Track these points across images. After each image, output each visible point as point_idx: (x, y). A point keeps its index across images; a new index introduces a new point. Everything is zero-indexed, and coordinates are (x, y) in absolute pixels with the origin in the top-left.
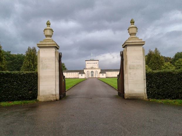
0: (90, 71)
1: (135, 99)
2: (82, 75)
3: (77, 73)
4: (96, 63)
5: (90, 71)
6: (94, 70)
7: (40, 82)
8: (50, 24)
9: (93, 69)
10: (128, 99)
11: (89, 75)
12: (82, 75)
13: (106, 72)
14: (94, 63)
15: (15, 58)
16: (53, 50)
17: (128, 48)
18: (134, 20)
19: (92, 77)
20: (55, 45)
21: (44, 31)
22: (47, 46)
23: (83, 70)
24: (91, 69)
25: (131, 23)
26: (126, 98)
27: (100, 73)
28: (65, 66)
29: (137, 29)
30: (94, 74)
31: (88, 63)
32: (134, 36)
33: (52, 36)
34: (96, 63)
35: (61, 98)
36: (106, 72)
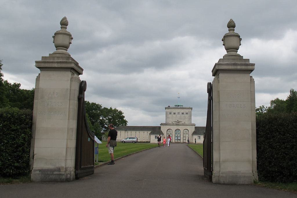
1: (232, 184)
3: (146, 132)
4: (187, 113)
5: (176, 127)
6: (182, 128)
7: (36, 140)
8: (234, 27)
9: (179, 125)
10: (218, 183)
14: (170, 113)
15: (28, 98)
16: (69, 74)
17: (221, 75)
18: (68, 20)
19: (176, 141)
20: (73, 65)
21: (54, 37)
22: (56, 65)
23: (160, 127)
24: (177, 125)
25: (229, 27)
26: (214, 180)
27: (194, 133)
28: (124, 117)
29: (240, 40)
30: (182, 136)
31: (170, 113)
32: (234, 53)
33: (70, 47)
34: (187, 113)
35: (77, 177)
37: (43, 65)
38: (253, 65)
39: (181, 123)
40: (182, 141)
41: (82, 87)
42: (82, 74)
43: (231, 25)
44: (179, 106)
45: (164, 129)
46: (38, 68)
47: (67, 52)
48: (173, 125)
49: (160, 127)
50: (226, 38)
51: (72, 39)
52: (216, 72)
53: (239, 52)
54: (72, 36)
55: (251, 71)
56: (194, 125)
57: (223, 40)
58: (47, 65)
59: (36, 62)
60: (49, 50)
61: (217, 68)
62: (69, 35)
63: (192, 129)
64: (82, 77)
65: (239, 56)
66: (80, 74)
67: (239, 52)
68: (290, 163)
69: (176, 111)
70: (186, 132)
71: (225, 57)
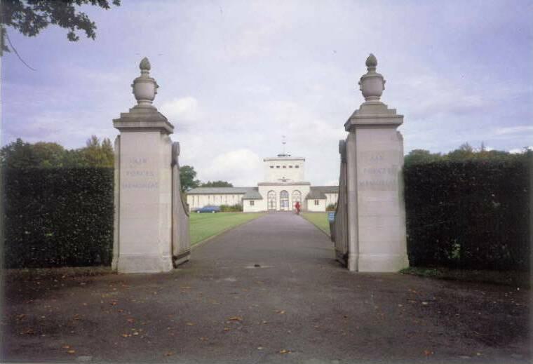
0: (278, 189)
2: (317, 203)
8: (148, 69)
11: (274, 204)
12: (317, 203)
13: (327, 195)
14: (272, 167)
17: (359, 132)
23: (256, 189)
29: (384, 82)
33: (156, 98)
34: (297, 167)
36: (327, 195)
37: (124, 125)
38: (402, 117)
39: (289, 182)
40: (278, 209)
41: (175, 151)
42: (172, 133)
43: (371, 63)
44: (284, 155)
45: (263, 191)
46: (118, 128)
47: (152, 105)
48: (275, 184)
49: (256, 189)
50: (138, 84)
51: (157, 87)
52: (351, 127)
53: (382, 100)
54: (385, 79)
55: (398, 125)
56: (308, 184)
57: (359, 84)
58: (131, 125)
59: (115, 121)
60: (127, 102)
61: (353, 122)
62: (380, 77)
63: (306, 190)
64: (174, 137)
65: (382, 104)
66: (169, 133)
67: (382, 100)
68: (425, 223)
69: (281, 164)
71: (363, 108)
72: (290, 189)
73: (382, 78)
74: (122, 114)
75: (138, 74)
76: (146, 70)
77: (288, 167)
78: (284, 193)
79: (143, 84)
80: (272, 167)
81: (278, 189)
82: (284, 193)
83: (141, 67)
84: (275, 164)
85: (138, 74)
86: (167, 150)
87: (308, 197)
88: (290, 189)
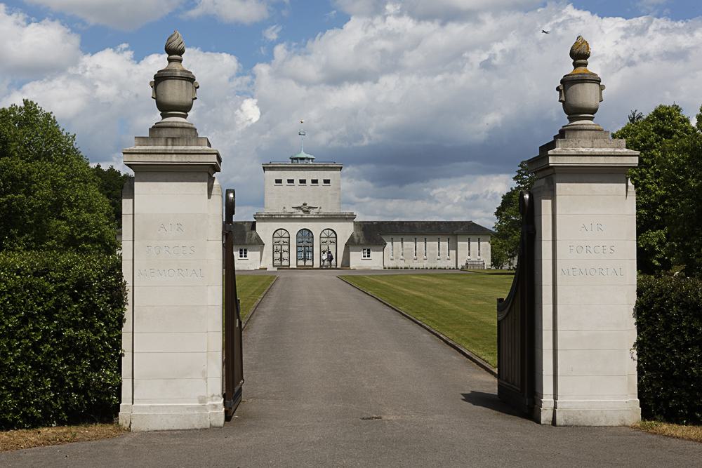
0: (293, 228)
11: (285, 255)
14: (279, 181)
29: (602, 88)
34: (327, 181)
48: (289, 218)
56: (349, 218)
63: (345, 231)
69: (297, 175)
70: (328, 237)
72: (316, 228)
73: (598, 81)
74: (635, 324)
75: (569, 68)
76: (583, 61)
77: (321, 181)
78: (306, 235)
79: (579, 87)
80: (279, 181)
81: (293, 228)
82: (306, 235)
83: (573, 55)
84: (285, 175)
85: (569, 68)
86: (216, 208)
87: (351, 244)
88: (316, 228)
